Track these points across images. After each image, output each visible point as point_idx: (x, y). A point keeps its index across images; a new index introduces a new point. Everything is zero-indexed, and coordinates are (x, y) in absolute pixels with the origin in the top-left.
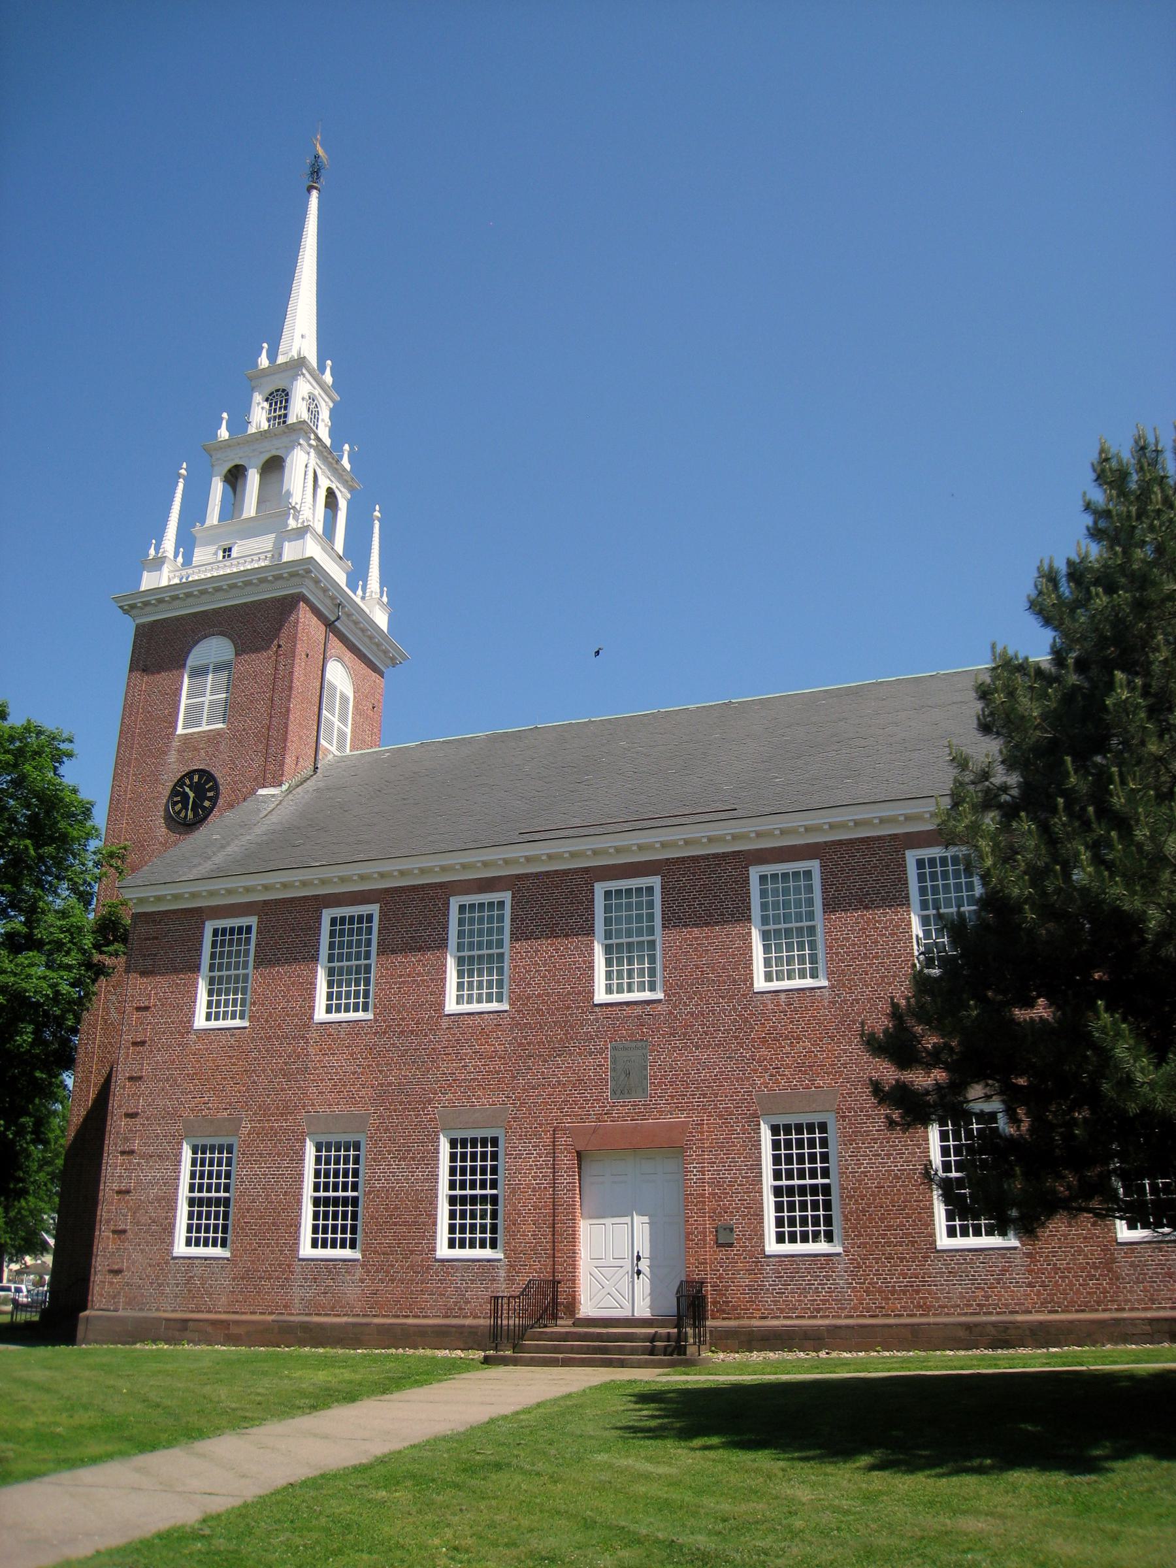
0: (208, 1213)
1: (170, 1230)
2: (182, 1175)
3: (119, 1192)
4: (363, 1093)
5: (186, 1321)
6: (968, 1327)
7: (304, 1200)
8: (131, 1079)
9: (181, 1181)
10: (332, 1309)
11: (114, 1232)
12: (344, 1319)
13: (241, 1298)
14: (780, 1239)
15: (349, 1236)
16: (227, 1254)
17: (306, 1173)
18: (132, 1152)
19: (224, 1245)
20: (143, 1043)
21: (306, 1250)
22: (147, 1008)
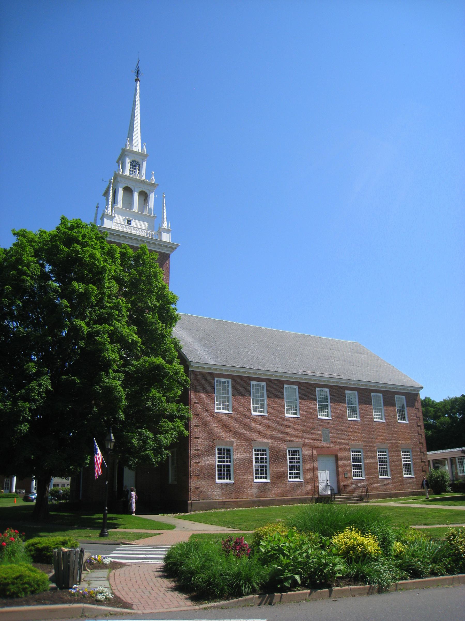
3: (196, 463)
4: (267, 436)
6: (386, 494)
8: (195, 426)
11: (195, 475)
12: (268, 499)
16: (233, 482)
18: (199, 450)
20: (198, 415)
22: (198, 403)
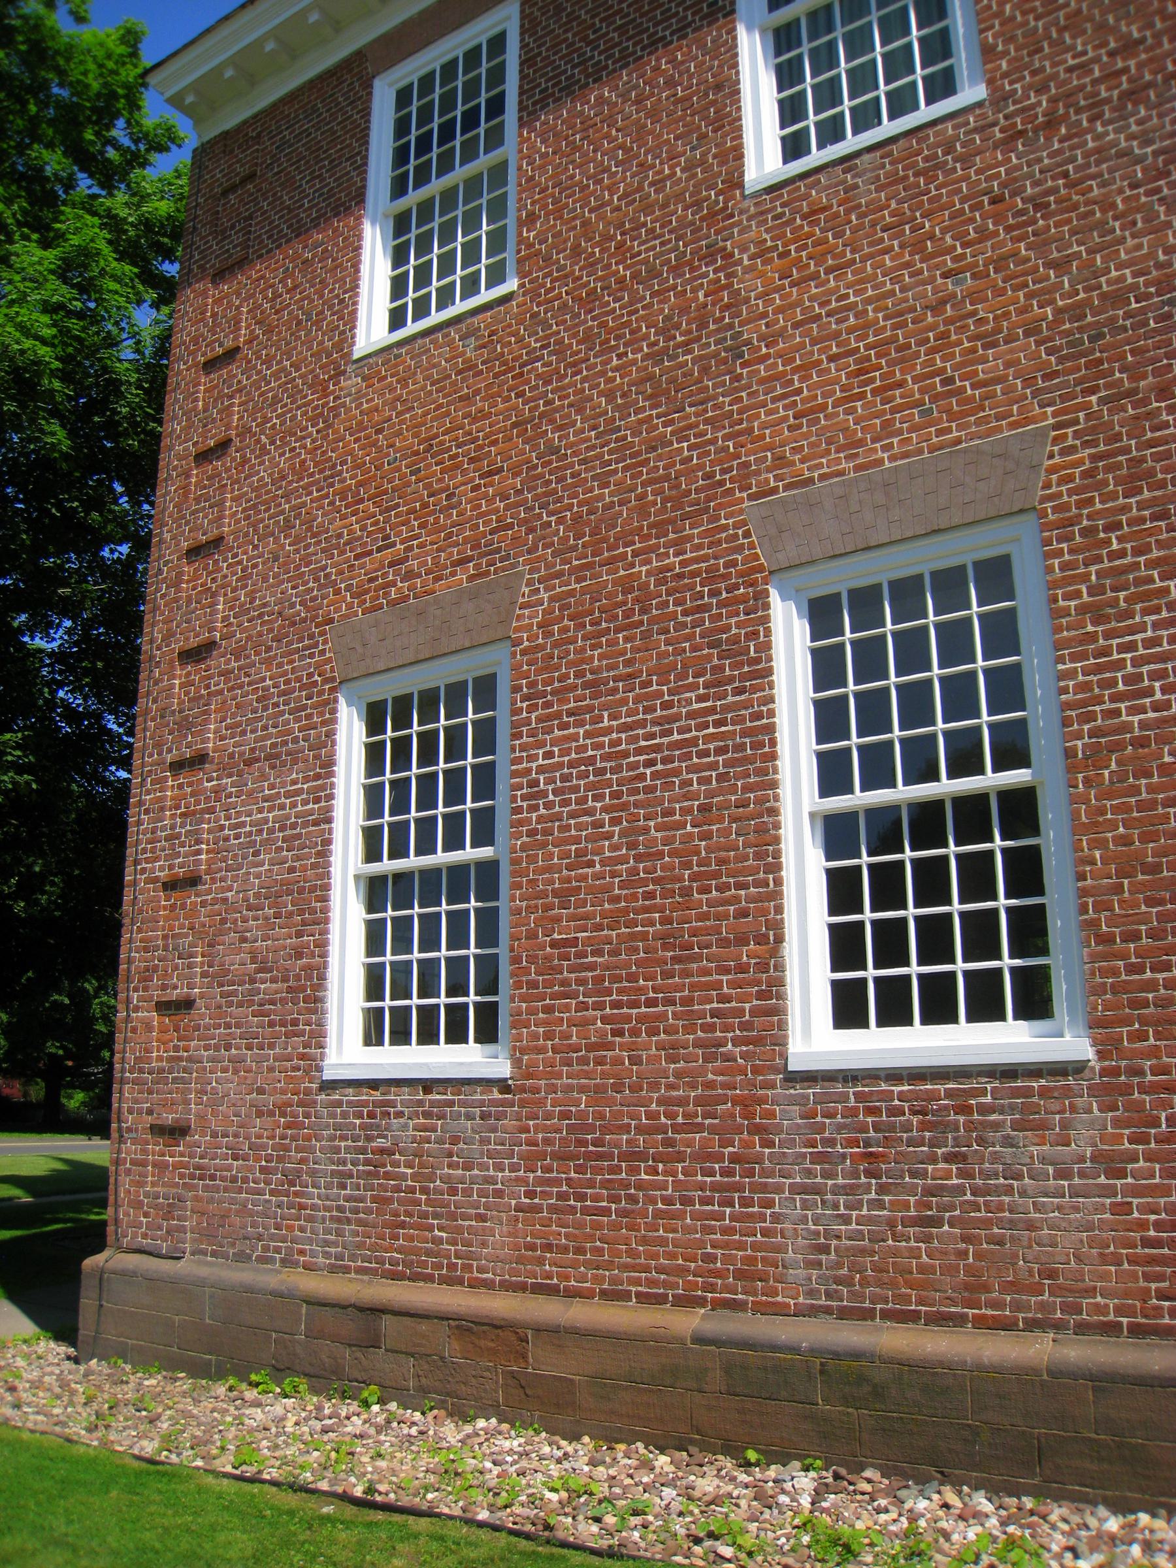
0: (430, 923)
1: (308, 988)
2: (339, 804)
3: (171, 886)
5: (376, 1311)
7: (787, 832)
9: (338, 826)
10: (973, 1290)
11: (163, 1007)
12: (1039, 1350)
13: (560, 1234)
14: (848, 1009)
15: (472, 998)
16: (502, 1068)
17: (782, 721)
18: (201, 759)
19: (488, 1035)
21: (814, 1036)
